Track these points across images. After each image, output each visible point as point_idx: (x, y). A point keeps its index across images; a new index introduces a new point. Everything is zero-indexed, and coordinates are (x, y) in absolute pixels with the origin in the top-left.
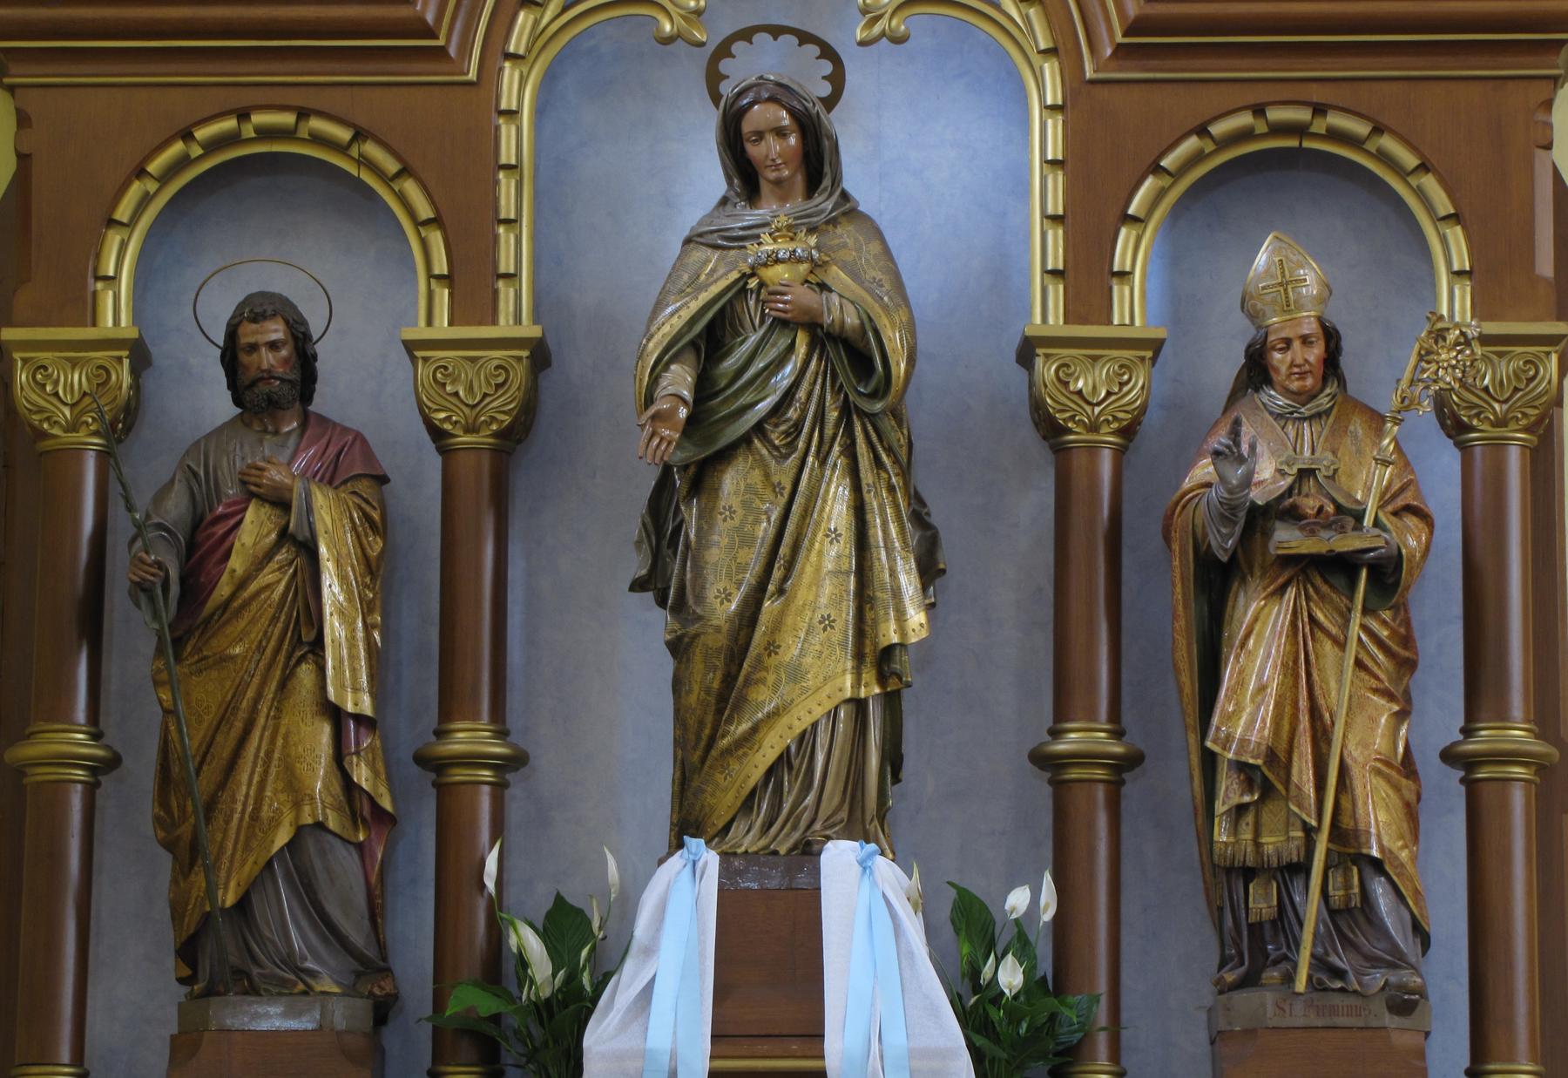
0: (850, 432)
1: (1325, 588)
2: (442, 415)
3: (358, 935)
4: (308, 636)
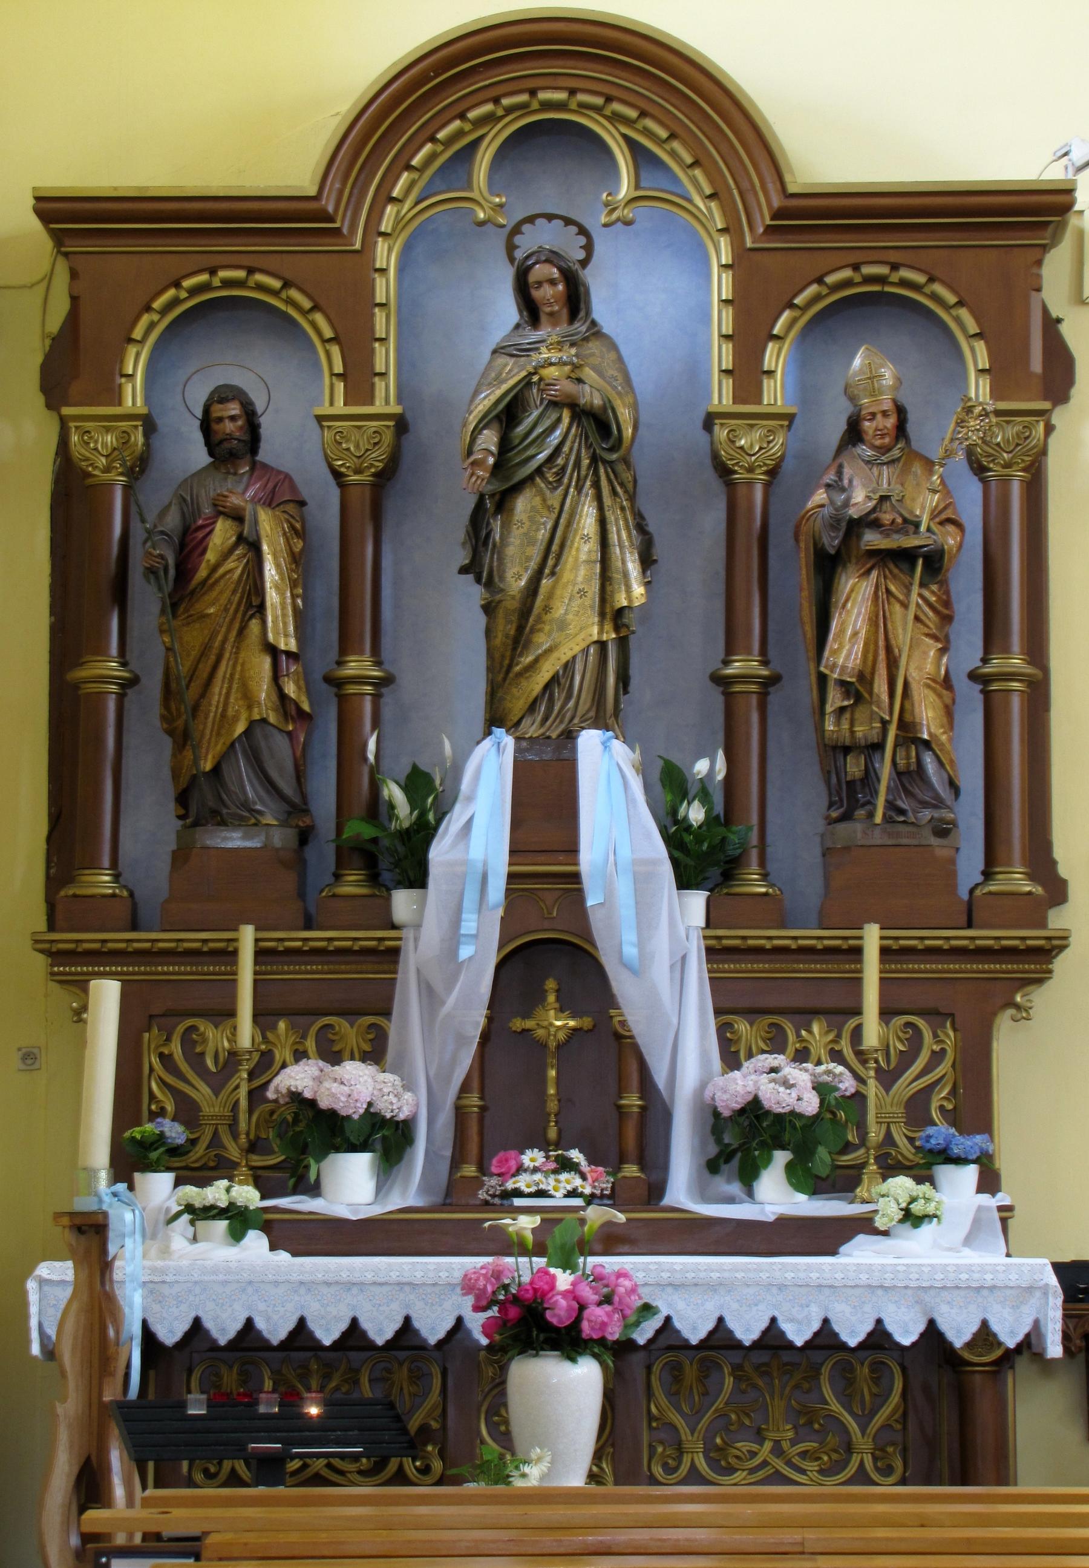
0: (596, 473)
1: (896, 571)
2: (340, 463)
3: (287, 787)
4: (255, 602)
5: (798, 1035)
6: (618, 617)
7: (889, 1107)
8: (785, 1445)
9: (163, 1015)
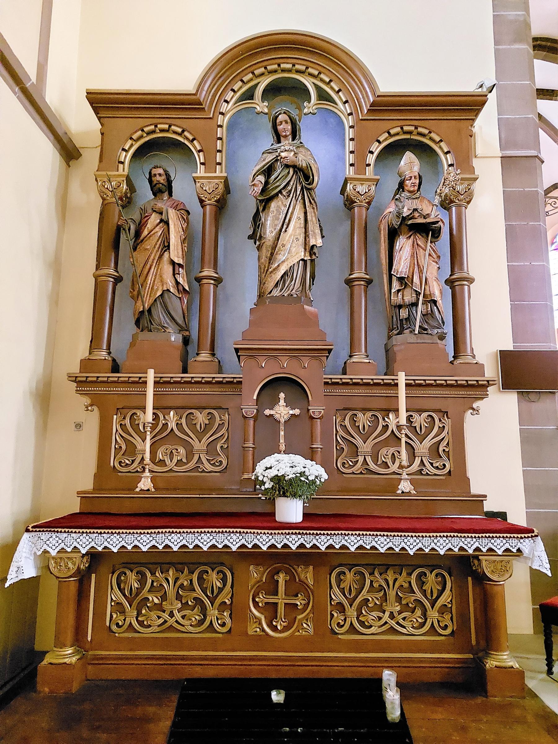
0: (303, 194)
1: (420, 237)
3: (180, 321)
4: (166, 244)
5: (384, 419)
6: (311, 250)
7: (422, 450)
8: (396, 614)
9: (123, 408)
